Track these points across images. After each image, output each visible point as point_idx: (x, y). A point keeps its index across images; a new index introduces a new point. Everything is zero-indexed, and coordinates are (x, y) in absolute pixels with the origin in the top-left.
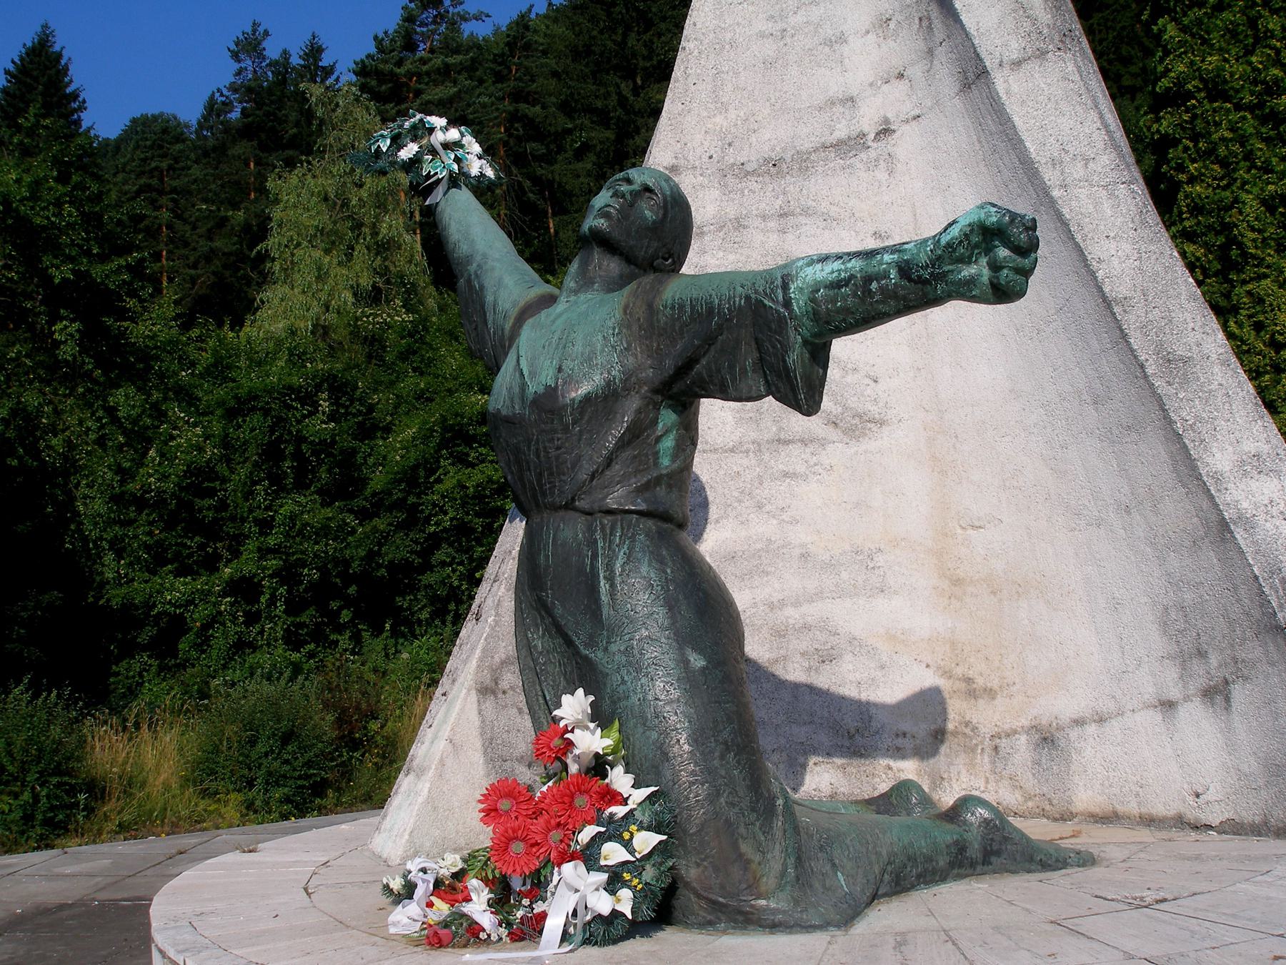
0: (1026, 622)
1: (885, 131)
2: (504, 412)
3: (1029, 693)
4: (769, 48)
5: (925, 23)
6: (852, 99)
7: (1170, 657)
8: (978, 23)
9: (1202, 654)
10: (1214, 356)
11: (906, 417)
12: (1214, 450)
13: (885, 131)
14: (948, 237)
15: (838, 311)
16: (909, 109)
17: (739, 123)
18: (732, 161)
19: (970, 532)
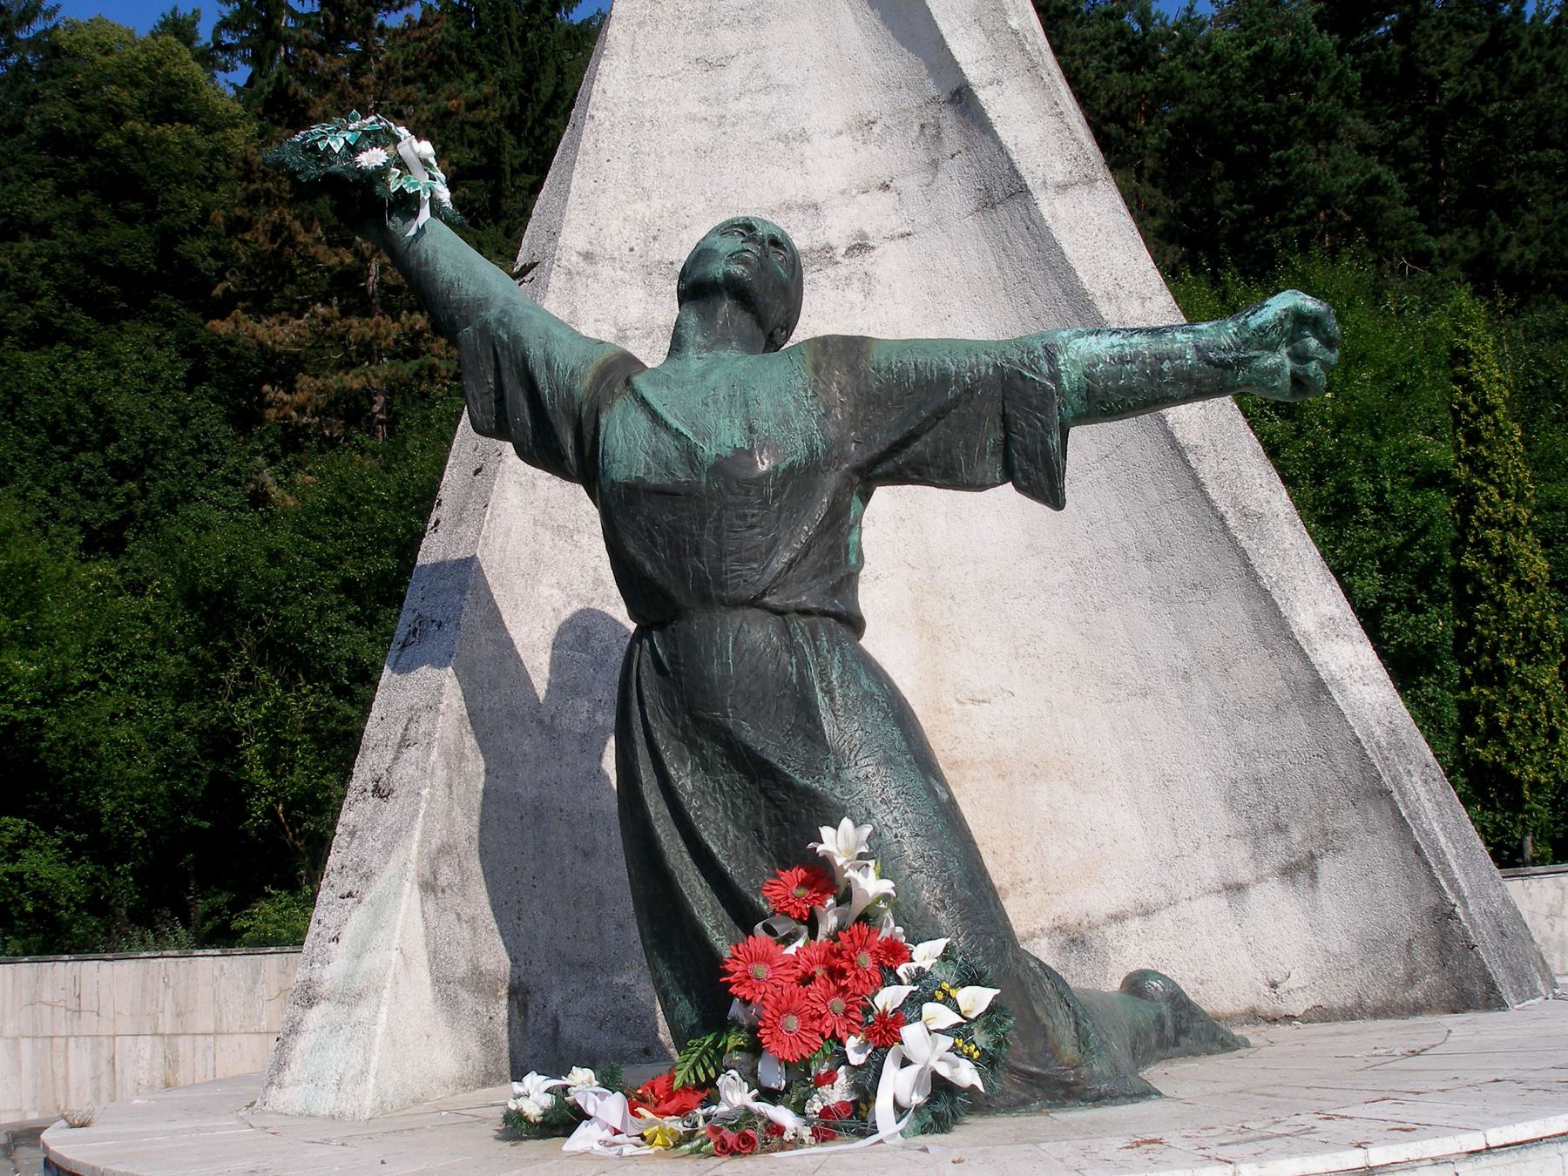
0: (1045, 808)
1: (860, 247)
2: (653, 480)
3: (1049, 890)
4: (703, 135)
5: (929, 131)
6: (815, 206)
7: (1238, 835)
8: (1016, 137)
9: (1280, 828)
10: (1282, 516)
11: (886, 574)
12: (1299, 610)
13: (860, 247)
14: (1260, 321)
15: (1119, 390)
16: (895, 224)
17: (665, 214)
18: (658, 257)
19: (969, 707)
